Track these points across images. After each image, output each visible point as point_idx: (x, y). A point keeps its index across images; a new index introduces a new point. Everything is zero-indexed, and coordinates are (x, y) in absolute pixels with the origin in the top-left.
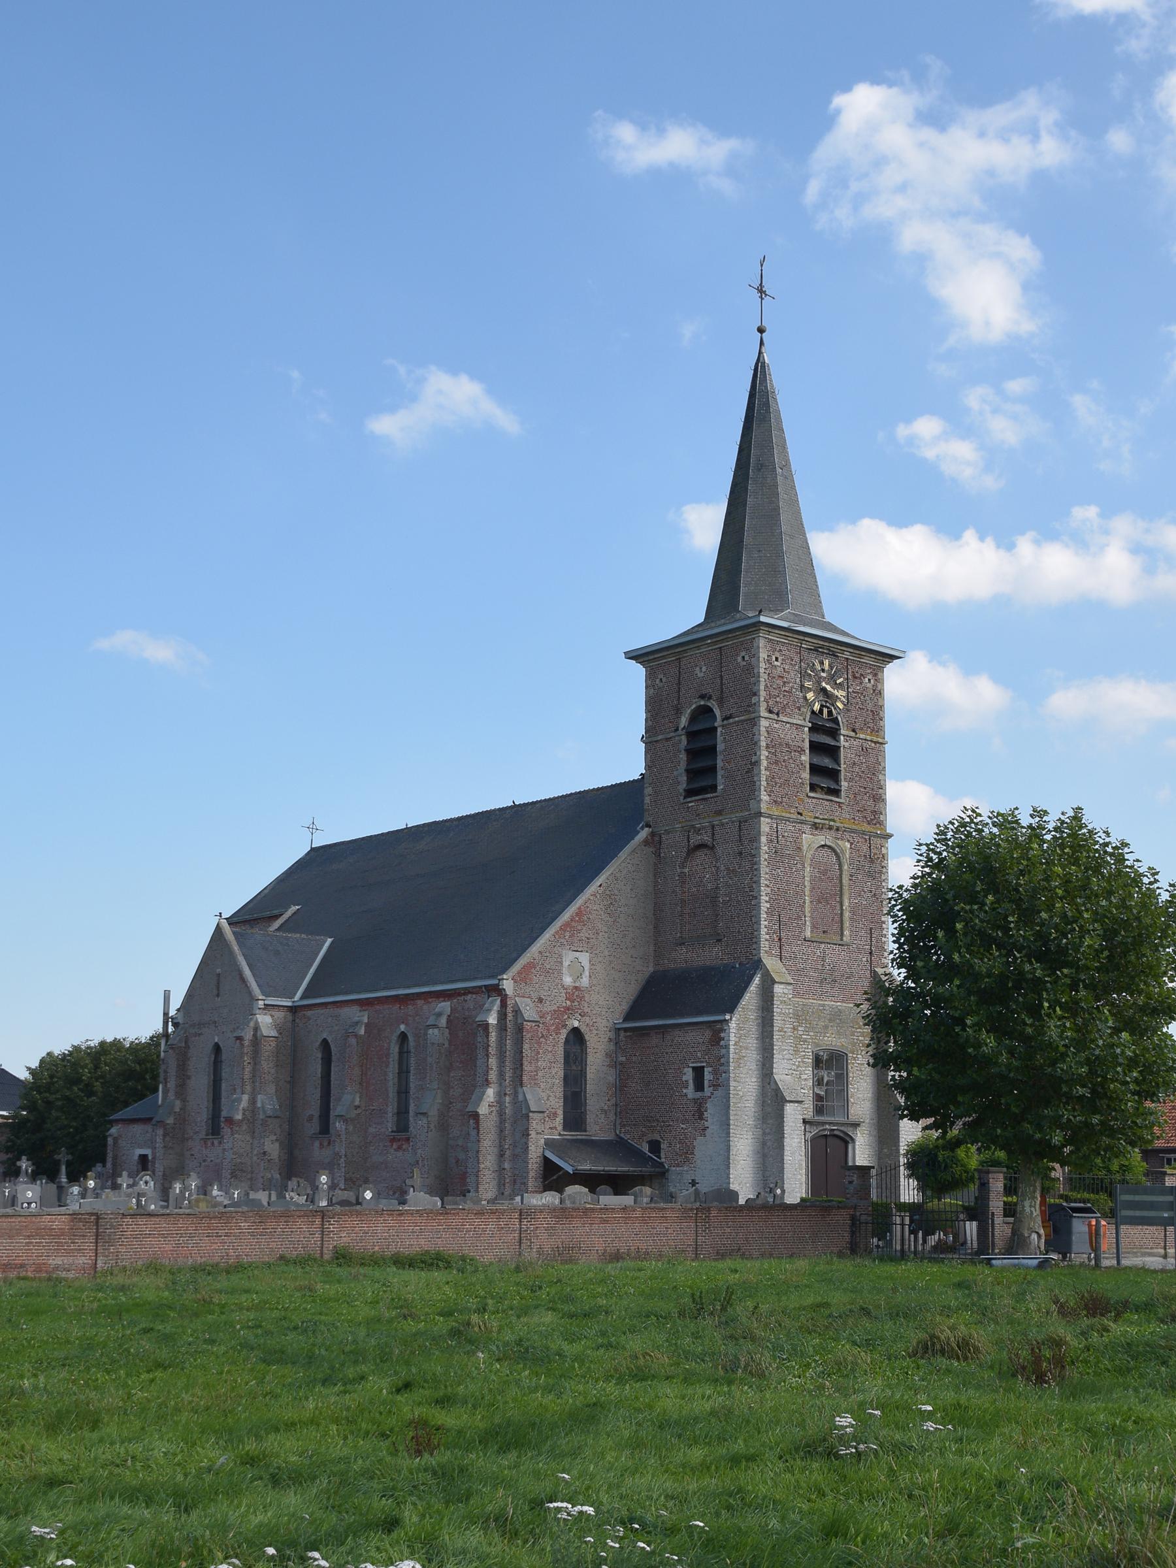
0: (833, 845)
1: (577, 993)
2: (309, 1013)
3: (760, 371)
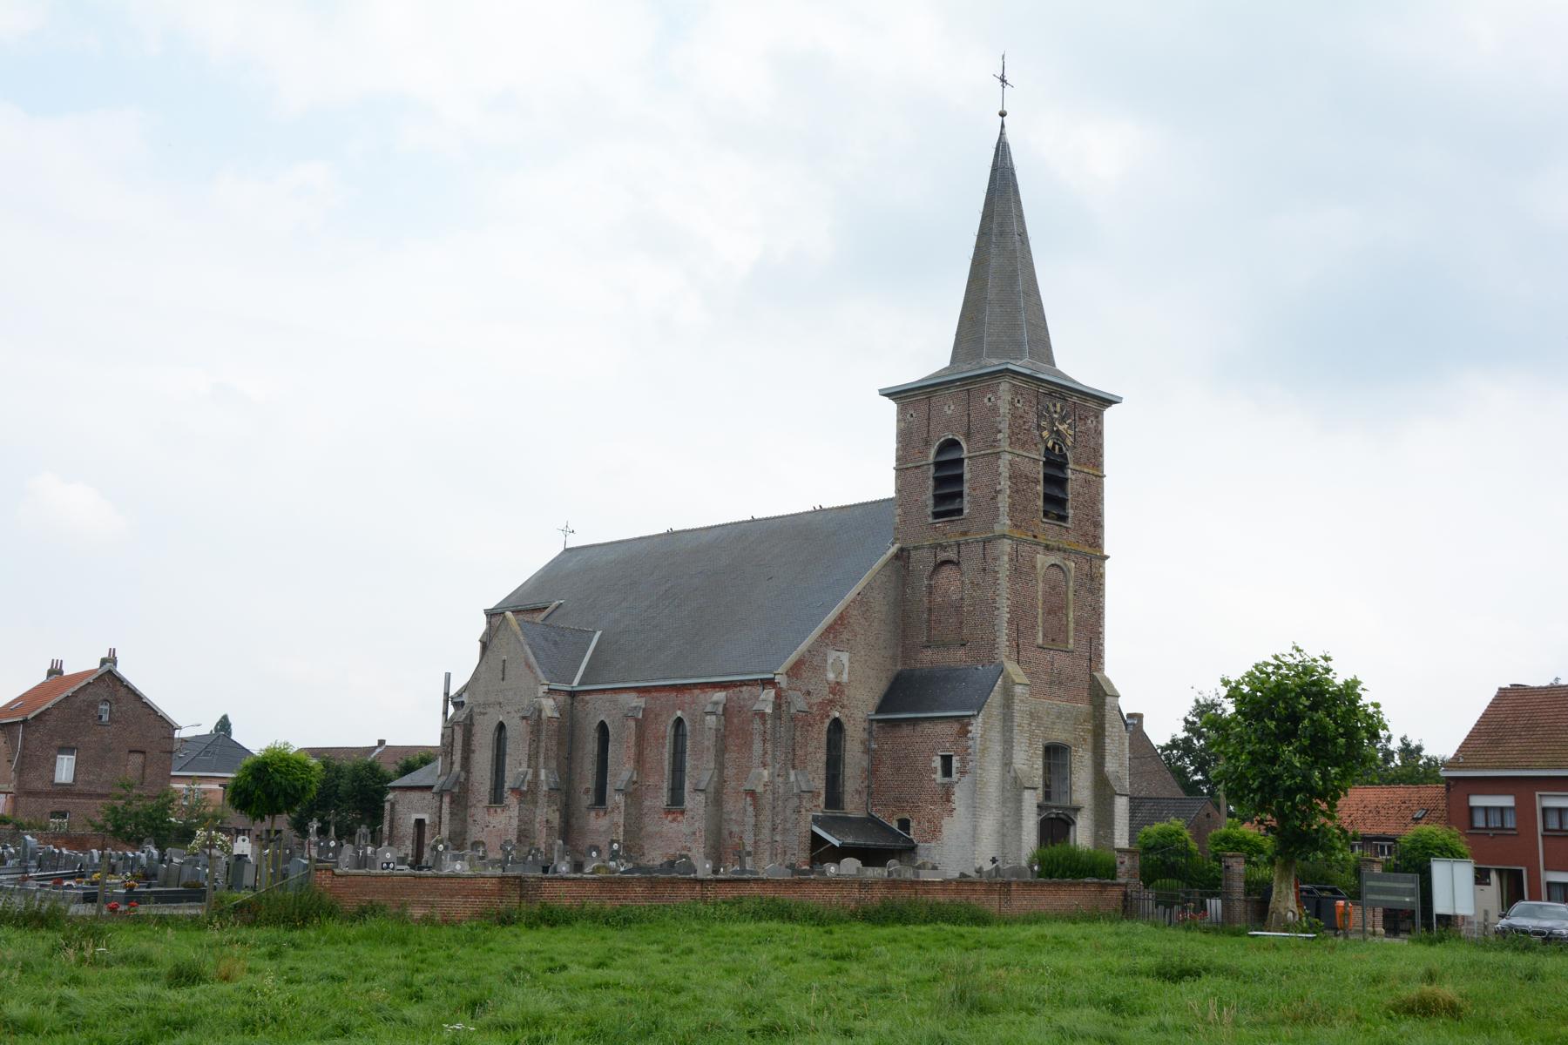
0: (1062, 565)
1: (838, 688)
2: (587, 698)
3: (1002, 149)
